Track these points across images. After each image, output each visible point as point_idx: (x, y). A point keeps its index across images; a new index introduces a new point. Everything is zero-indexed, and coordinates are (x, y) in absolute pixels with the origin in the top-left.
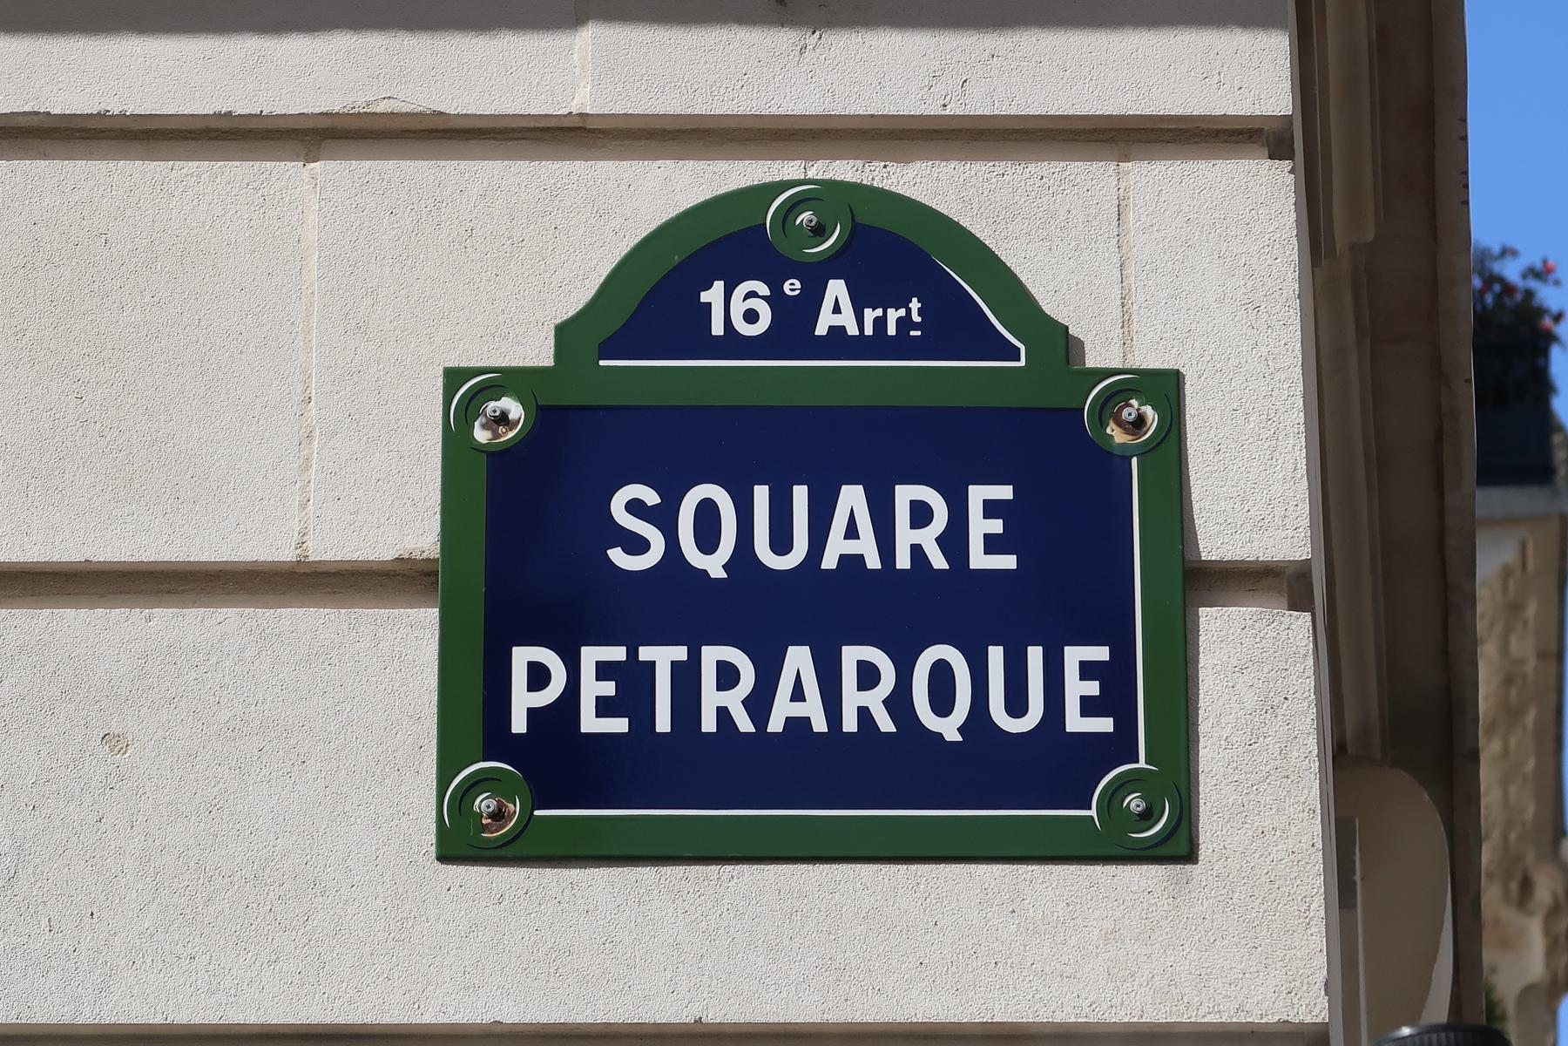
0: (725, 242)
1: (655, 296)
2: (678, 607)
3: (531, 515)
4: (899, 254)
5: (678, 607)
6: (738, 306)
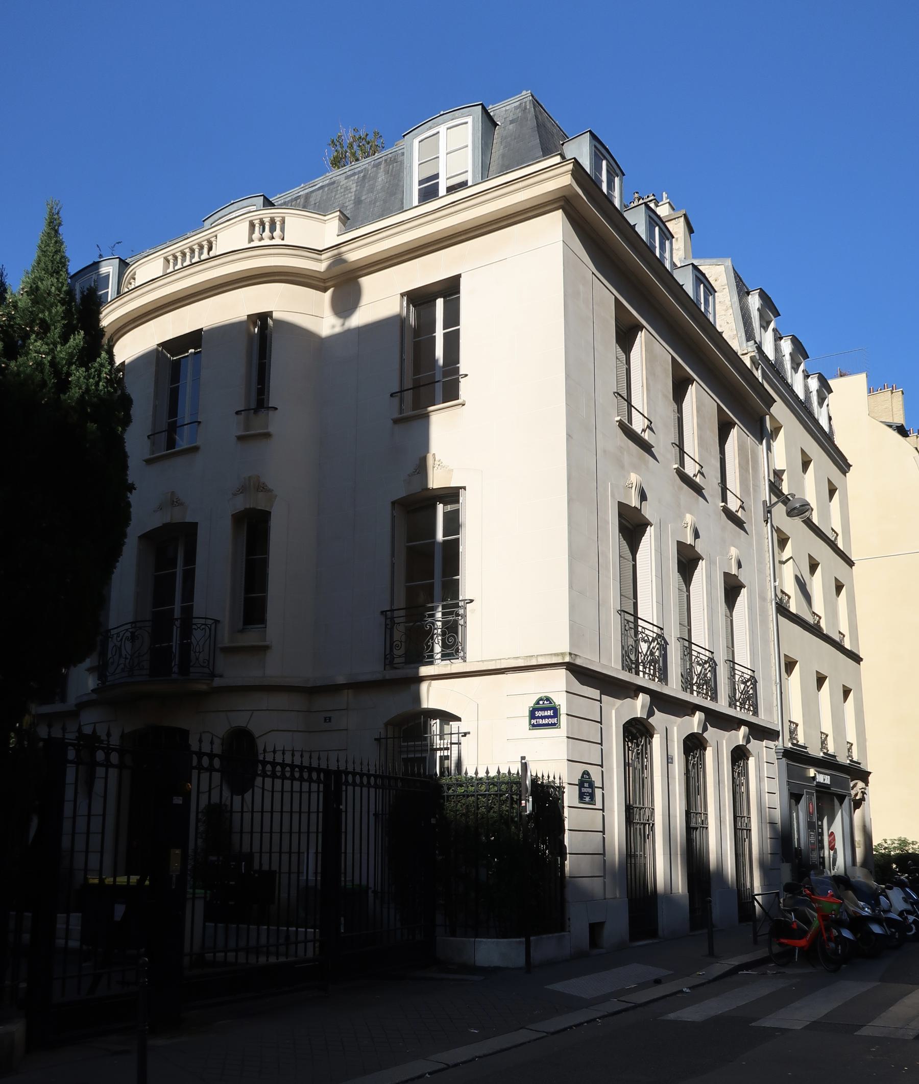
0: (541, 699)
1: (537, 703)
2: (539, 717)
3: (532, 715)
4: (548, 699)
5: (539, 717)
6: (541, 702)
